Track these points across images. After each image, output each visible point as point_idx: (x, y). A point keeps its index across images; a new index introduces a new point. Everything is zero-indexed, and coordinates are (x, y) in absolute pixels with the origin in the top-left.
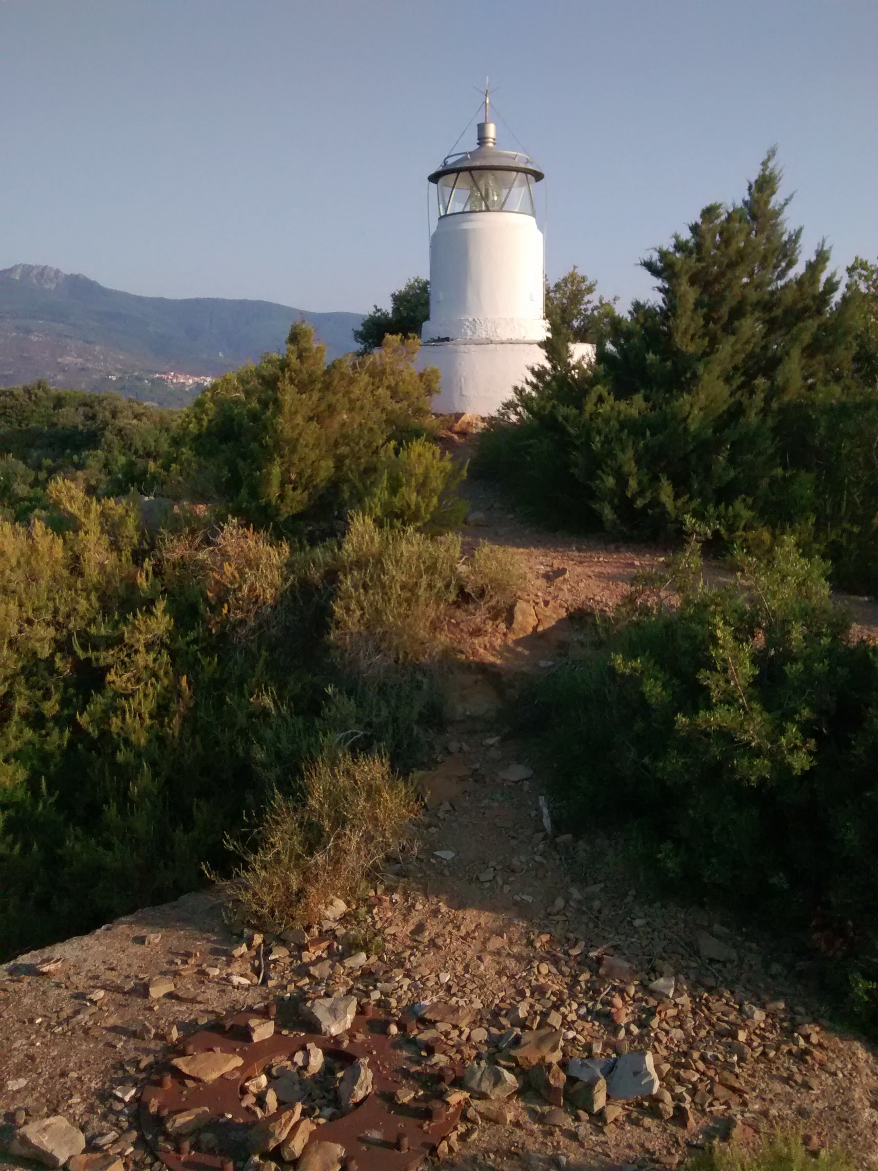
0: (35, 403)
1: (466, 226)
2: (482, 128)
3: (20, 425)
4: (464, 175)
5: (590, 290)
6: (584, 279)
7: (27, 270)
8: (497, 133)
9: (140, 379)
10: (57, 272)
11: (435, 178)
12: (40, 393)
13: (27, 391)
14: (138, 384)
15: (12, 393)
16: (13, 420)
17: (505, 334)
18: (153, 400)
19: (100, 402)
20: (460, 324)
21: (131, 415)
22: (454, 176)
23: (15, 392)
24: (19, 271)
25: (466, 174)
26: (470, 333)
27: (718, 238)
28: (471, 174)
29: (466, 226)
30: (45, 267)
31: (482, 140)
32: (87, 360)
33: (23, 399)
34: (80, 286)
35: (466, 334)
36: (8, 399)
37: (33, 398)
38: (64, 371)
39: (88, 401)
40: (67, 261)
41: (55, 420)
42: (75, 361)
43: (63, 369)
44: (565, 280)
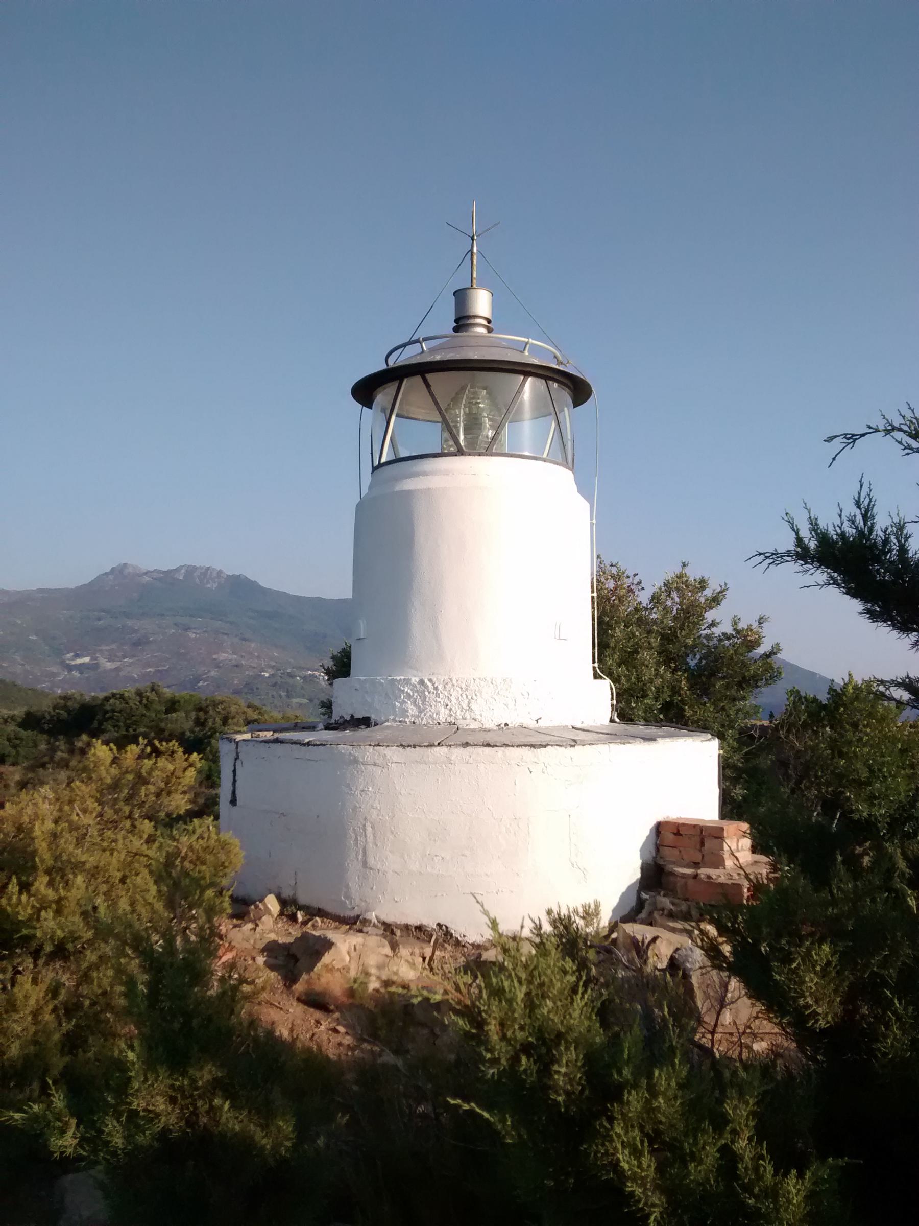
0: (146, 706)
1: (409, 485)
2: (461, 297)
3: (127, 730)
4: (413, 384)
5: (715, 600)
6: (702, 584)
7: (191, 571)
8: (495, 305)
9: (291, 676)
10: (220, 572)
11: (365, 391)
12: (153, 696)
13: (139, 694)
14: (290, 681)
15: (122, 697)
16: (121, 724)
17: (489, 714)
18: (303, 696)
19: (215, 704)
20: (392, 690)
21: (241, 721)
22: (391, 388)
23: (126, 694)
24: (183, 571)
25: (418, 379)
26: (412, 710)
27: (21, 836)
28: (431, 386)
29: (409, 485)
30: (208, 568)
31: (463, 322)
32: (242, 656)
33: (134, 702)
34: (241, 586)
35: (405, 712)
36: (118, 702)
37: (145, 701)
38: (218, 667)
39: (204, 704)
40: (230, 563)
41: (163, 725)
42: (230, 657)
43: (217, 665)
44: (668, 587)
